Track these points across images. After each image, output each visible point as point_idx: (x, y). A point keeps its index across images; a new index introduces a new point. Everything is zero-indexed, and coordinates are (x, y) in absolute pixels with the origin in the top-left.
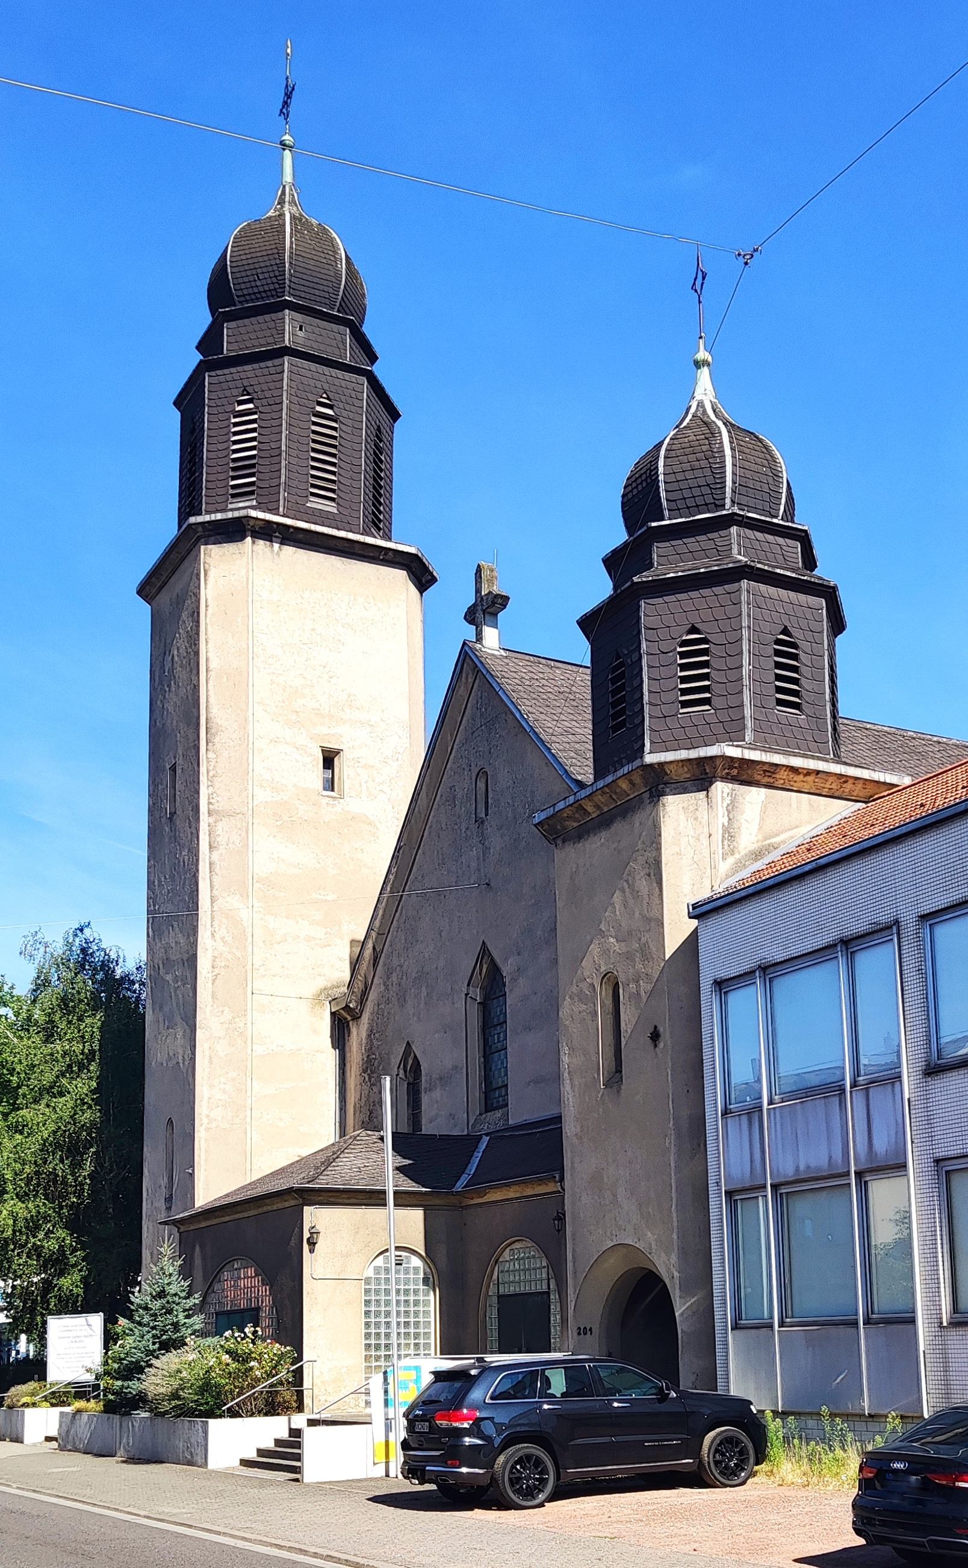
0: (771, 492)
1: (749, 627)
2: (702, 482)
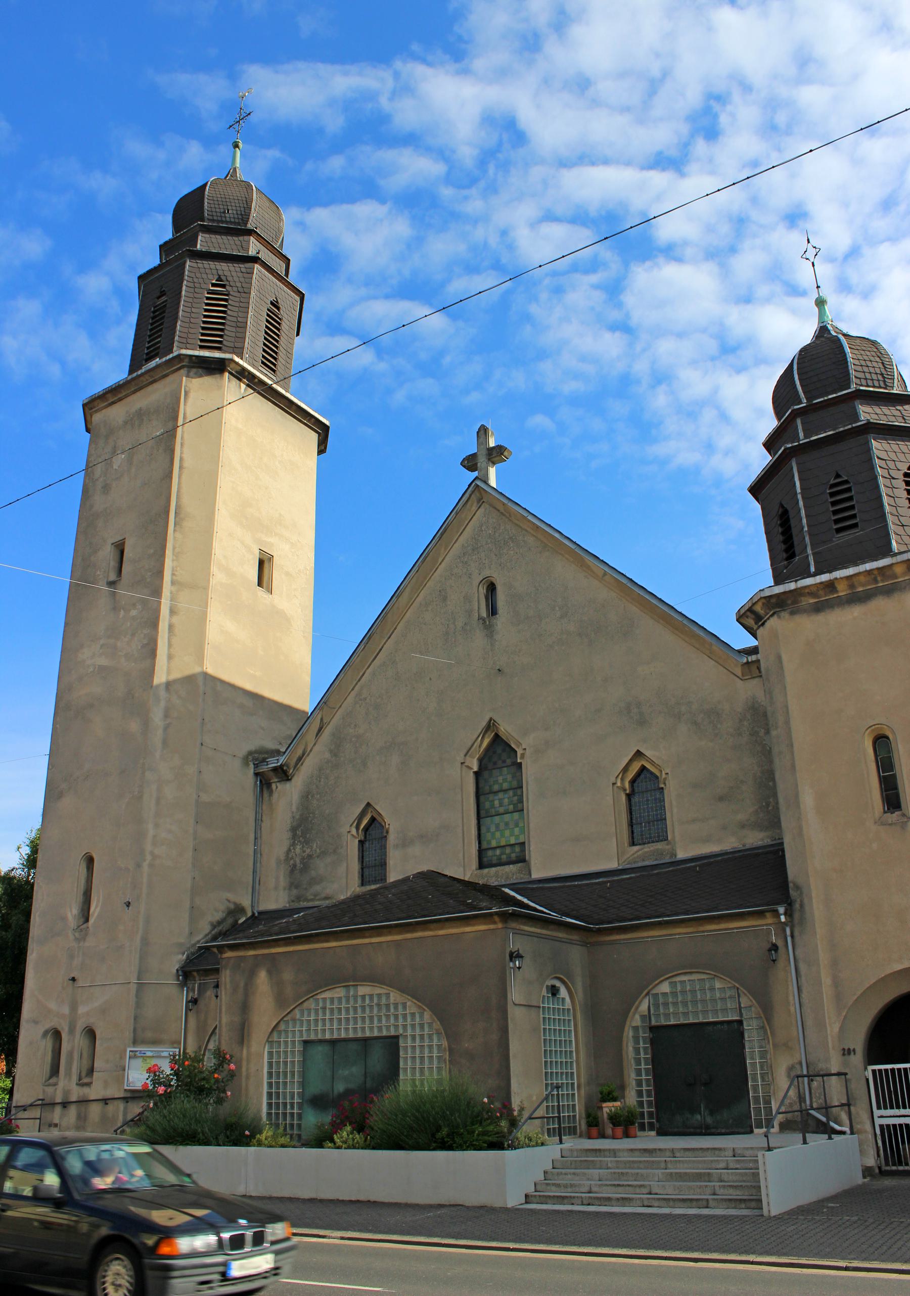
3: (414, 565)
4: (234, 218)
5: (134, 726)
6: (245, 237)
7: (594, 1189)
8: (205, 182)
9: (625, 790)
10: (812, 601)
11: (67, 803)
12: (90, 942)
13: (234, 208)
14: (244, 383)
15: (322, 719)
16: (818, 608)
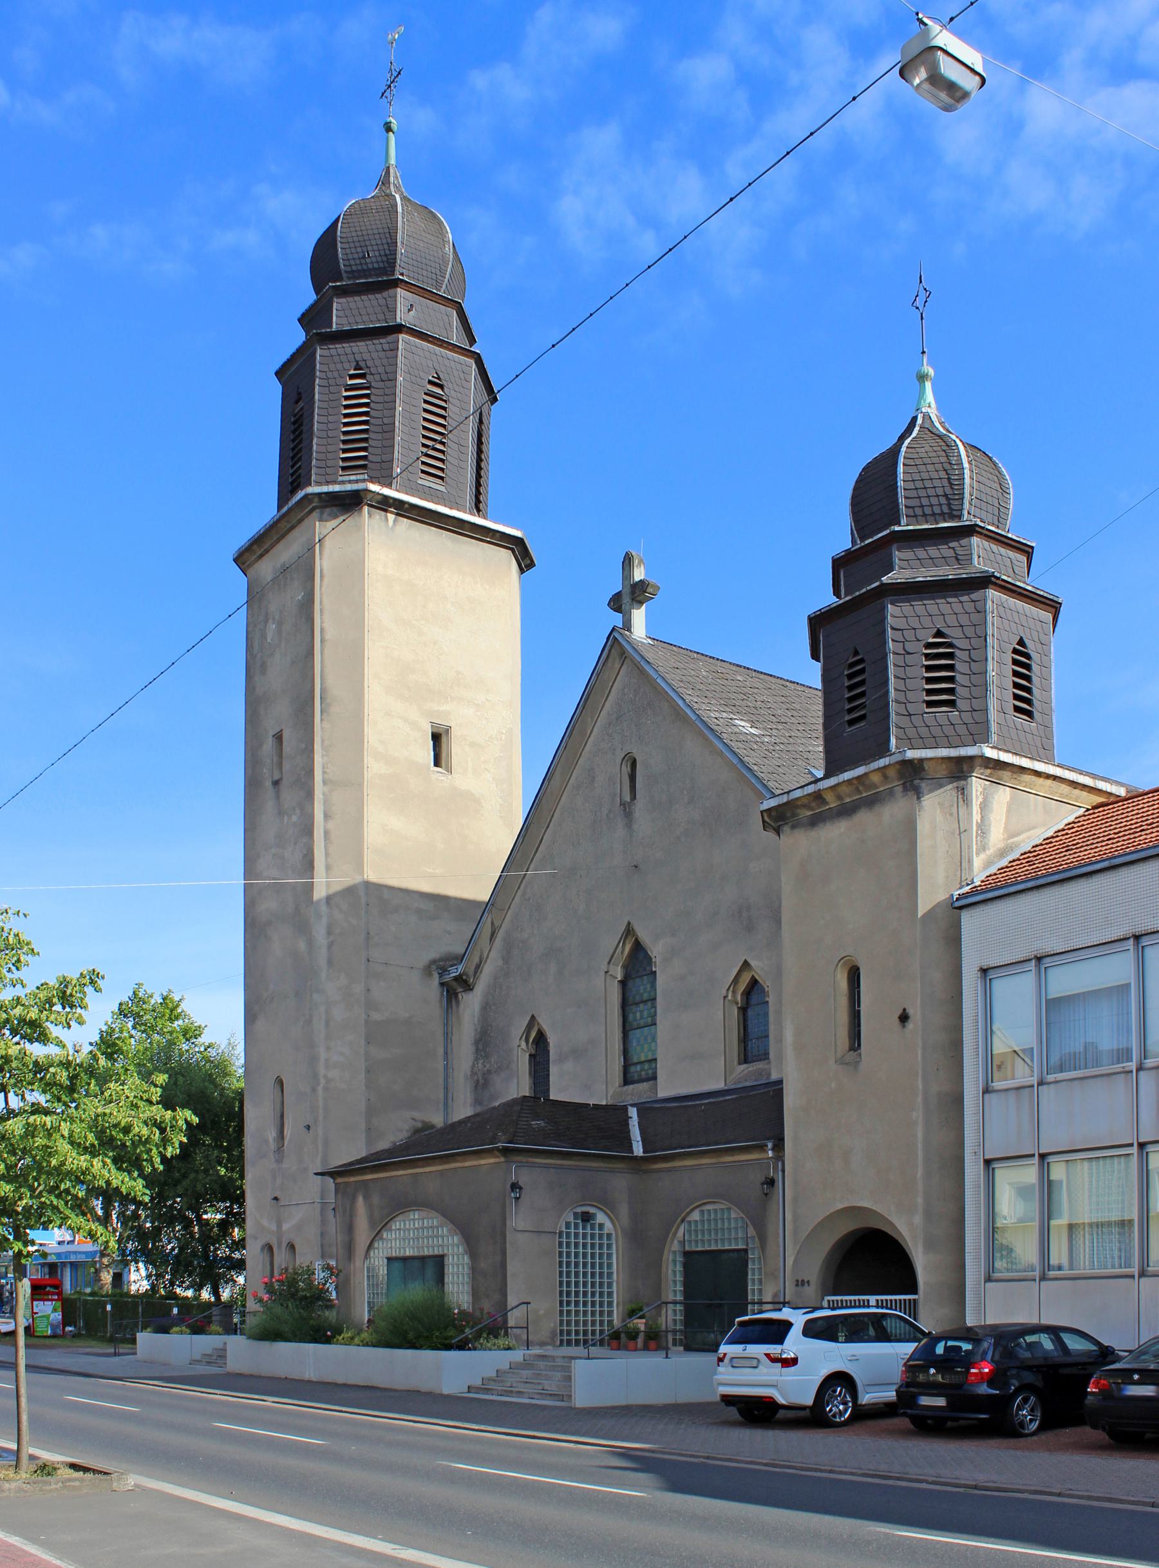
1: (993, 635)
2: (940, 492)
3: (563, 738)
5: (302, 946)
6: (390, 291)
7: (514, 1384)
8: (334, 219)
9: (737, 1003)
10: (809, 813)
11: (260, 1024)
12: (285, 1165)
13: (375, 248)
14: (391, 512)
15: (492, 924)
16: (815, 822)
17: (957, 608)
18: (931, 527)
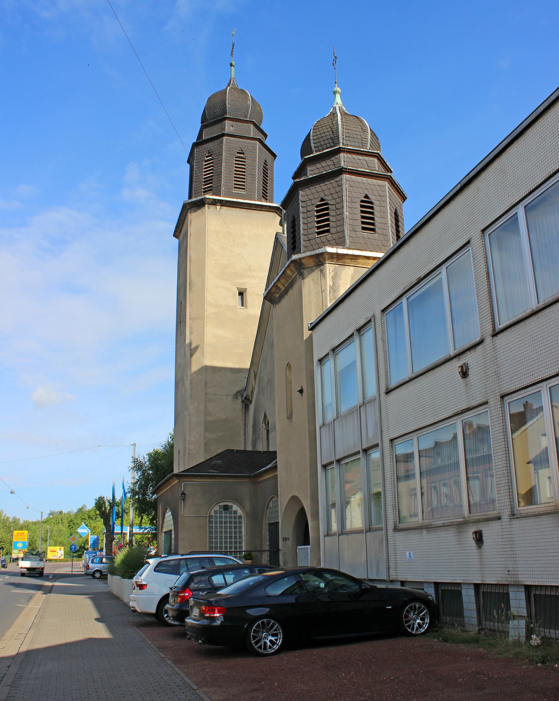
0: (362, 139)
2: (328, 137)
4: (220, 113)
15: (254, 371)
17: (330, 186)
18: (320, 153)
